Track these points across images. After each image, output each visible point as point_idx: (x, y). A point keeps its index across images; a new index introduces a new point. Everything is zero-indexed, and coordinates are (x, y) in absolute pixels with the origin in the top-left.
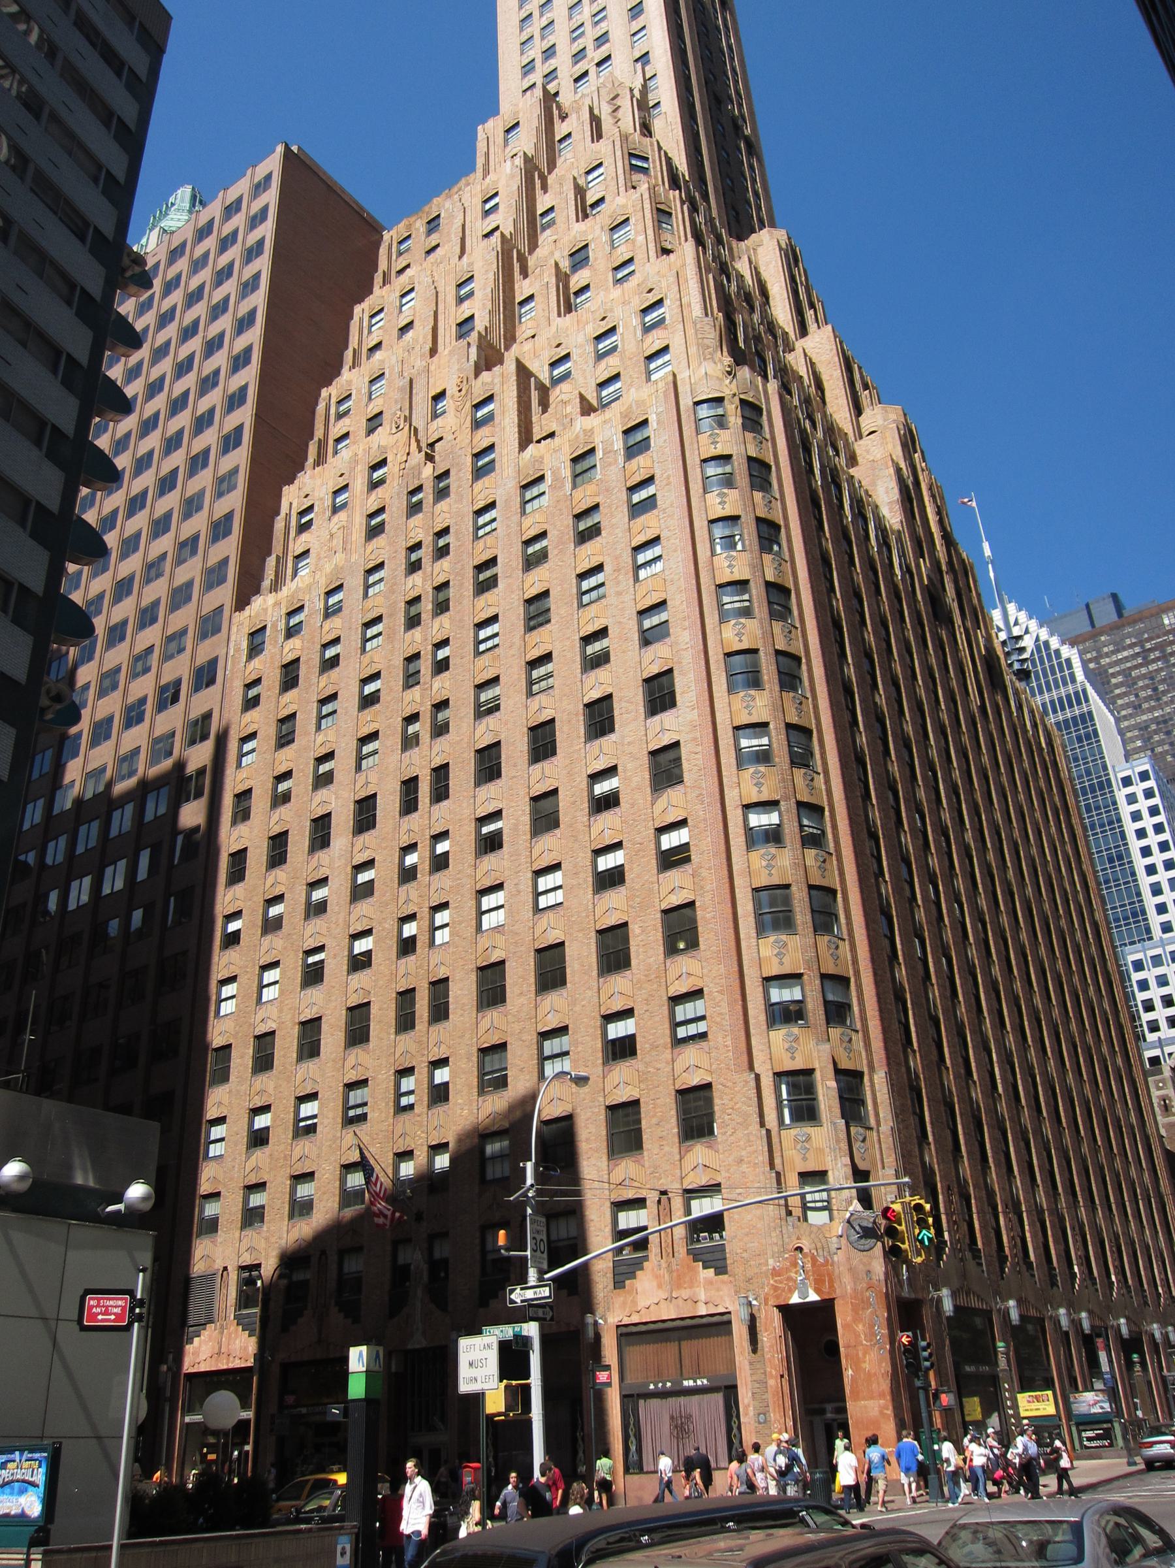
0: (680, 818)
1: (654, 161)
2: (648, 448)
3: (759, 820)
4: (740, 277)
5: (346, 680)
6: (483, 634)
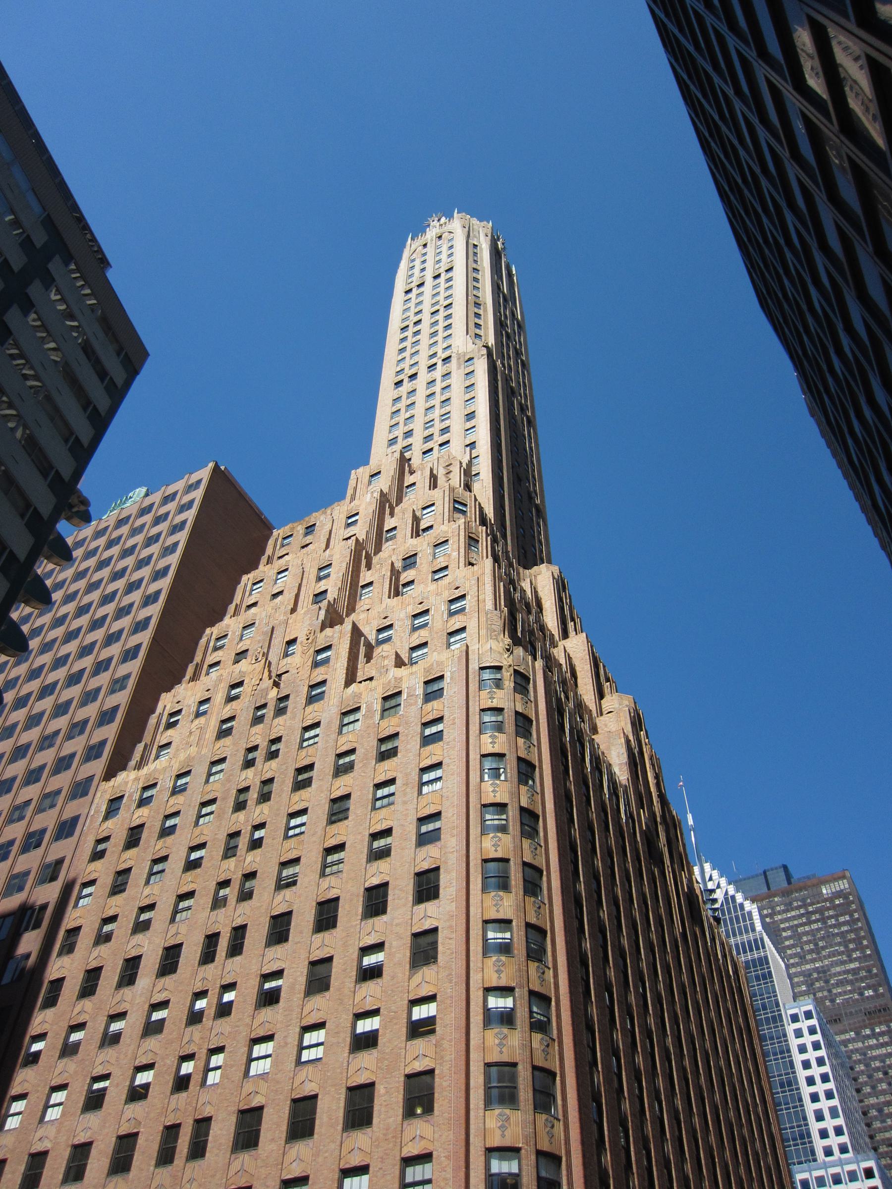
0: (431, 993)
1: (471, 507)
2: (441, 696)
3: (497, 1002)
4: (523, 591)
5: (177, 848)
6: (293, 823)
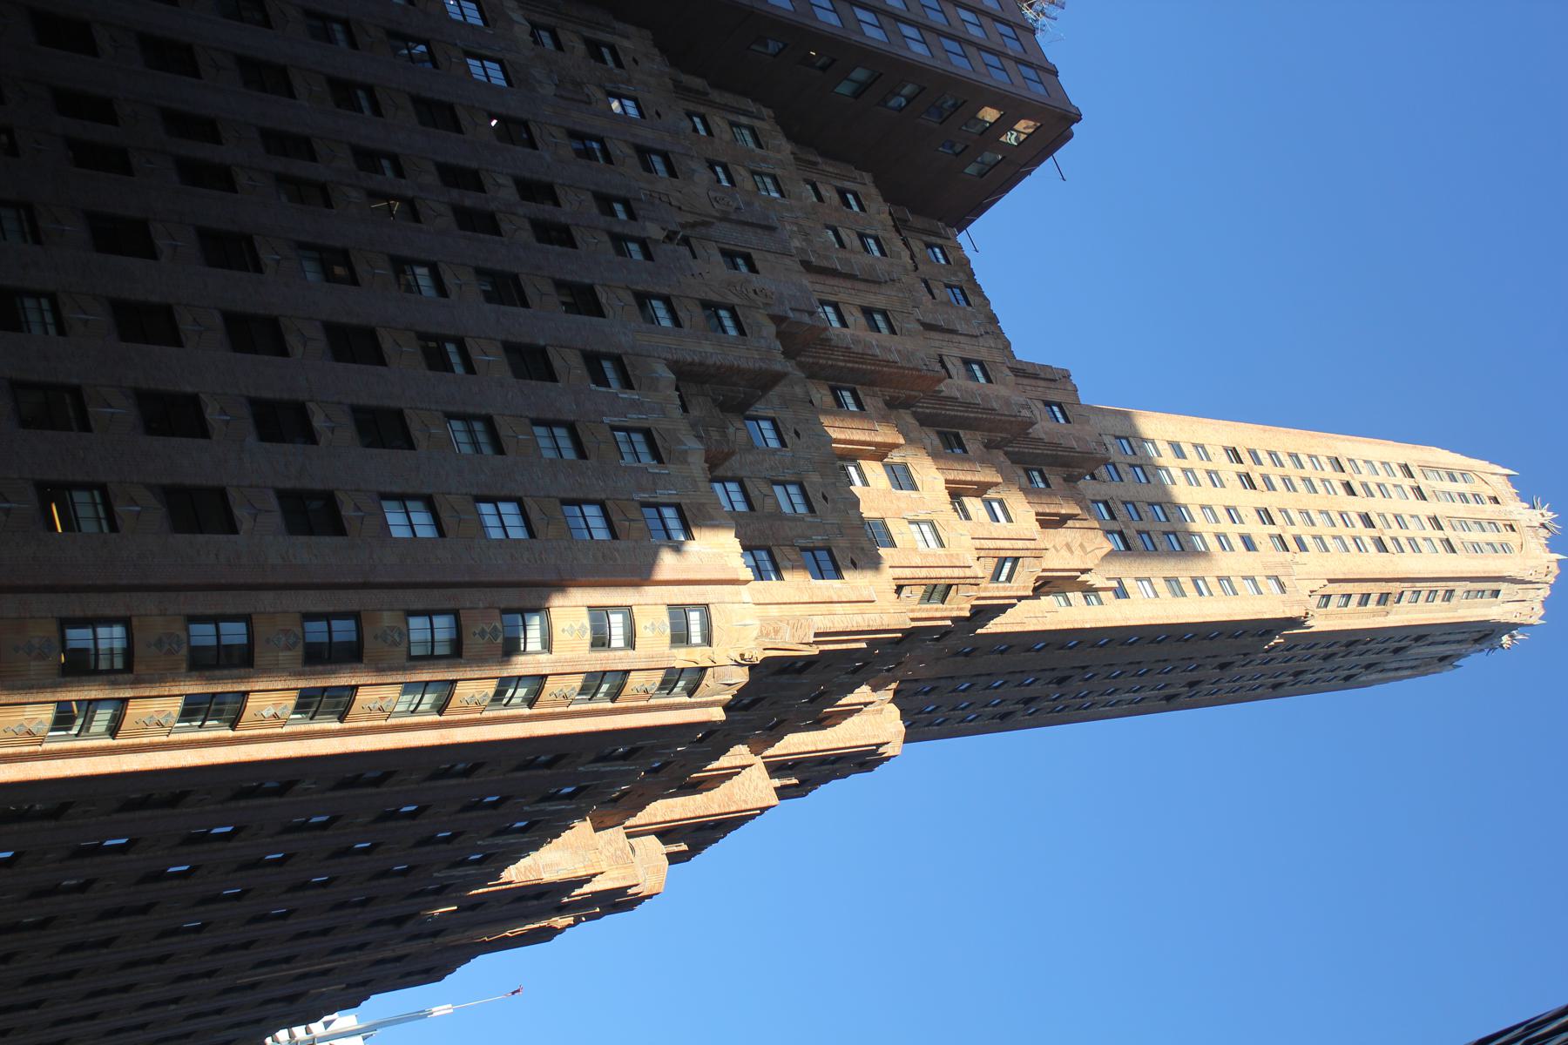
1: (1005, 589)
